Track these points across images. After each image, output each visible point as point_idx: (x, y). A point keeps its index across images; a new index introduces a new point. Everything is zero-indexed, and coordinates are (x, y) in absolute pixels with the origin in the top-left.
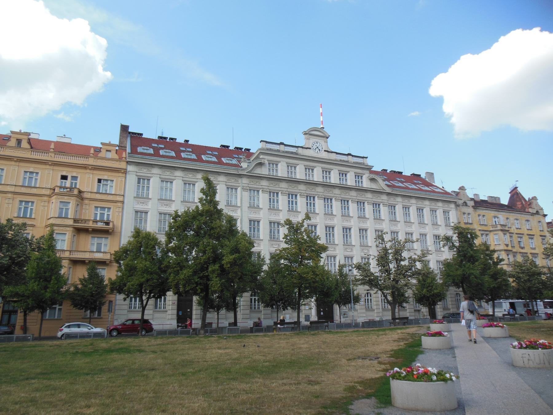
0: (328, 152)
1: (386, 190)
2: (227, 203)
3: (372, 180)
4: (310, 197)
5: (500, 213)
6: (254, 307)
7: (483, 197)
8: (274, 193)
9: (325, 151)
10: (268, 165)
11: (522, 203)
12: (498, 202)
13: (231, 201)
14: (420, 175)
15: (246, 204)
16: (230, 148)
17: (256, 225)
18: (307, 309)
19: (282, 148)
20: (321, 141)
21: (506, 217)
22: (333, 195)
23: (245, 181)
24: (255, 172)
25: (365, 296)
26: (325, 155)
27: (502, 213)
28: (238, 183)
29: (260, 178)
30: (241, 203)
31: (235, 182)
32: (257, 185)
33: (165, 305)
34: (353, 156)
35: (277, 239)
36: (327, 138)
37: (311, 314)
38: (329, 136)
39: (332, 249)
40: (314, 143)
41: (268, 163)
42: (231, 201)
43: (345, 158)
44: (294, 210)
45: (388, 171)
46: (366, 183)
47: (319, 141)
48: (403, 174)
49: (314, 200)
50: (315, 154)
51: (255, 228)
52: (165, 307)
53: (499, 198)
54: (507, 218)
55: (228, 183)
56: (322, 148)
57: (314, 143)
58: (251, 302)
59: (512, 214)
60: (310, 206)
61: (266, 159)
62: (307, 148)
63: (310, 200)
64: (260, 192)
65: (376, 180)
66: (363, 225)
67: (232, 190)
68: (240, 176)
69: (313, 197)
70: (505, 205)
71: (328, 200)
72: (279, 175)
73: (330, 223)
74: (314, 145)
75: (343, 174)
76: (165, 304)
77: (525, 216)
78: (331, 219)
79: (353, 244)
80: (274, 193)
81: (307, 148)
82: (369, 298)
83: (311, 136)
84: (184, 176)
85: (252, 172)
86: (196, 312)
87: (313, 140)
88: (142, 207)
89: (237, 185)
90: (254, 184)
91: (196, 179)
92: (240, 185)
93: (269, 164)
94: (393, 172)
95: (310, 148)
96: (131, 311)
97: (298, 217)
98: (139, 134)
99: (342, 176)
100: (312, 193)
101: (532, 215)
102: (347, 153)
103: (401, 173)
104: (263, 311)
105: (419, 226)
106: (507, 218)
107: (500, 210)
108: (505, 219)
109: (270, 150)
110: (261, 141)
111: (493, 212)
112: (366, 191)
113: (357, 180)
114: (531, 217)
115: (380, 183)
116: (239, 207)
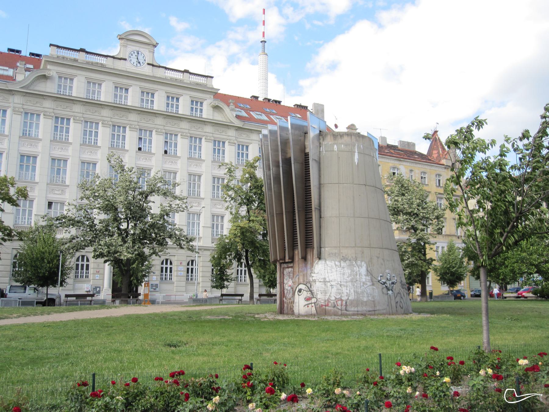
0: (153, 65)
1: (234, 123)
2: (112, 145)
3: (216, 108)
4: (219, 142)
5: (400, 163)
6: (165, 278)
7: (392, 141)
8: (196, 138)
9: (148, 64)
10: (57, 79)
11: (438, 153)
12: (411, 149)
13: (30, 131)
14: (307, 107)
15: (17, 132)
16: (259, 99)
17: (196, 180)
18: (98, 278)
19: (81, 57)
20: (145, 51)
21: (410, 168)
22: (153, 126)
23: (17, 100)
24: (37, 88)
25: (188, 264)
26: (147, 70)
27: (404, 163)
28: (8, 103)
29: (43, 96)
30: (10, 132)
31: (3, 101)
32: (36, 107)
33: (88, 274)
34: (88, 53)
35: (62, 183)
36: (155, 46)
37: (103, 286)
38: (157, 44)
39: (60, 192)
40: (132, 53)
41: (57, 77)
42: (30, 131)
43: (179, 76)
44: (120, 147)
45: (260, 99)
46: (207, 113)
47: (141, 50)
48: (282, 104)
49: (224, 146)
50: (134, 68)
51: (195, 184)
52: (88, 276)
53: (414, 145)
54: (411, 171)
55: (25, 106)
56: (145, 60)
57: (132, 53)
58: (162, 271)
59: (418, 166)
60: (243, 157)
61: (53, 71)
62: (120, 59)
63: (243, 150)
64: (42, 116)
65: (221, 108)
66: (172, 166)
67: (119, 128)
68: (11, 92)
69: (96, 123)
70: (421, 155)
71: (196, 141)
72: (74, 95)
73: (194, 169)
74: (132, 55)
75: (172, 98)
76: (88, 272)
77: (436, 169)
78: (32, 145)
79: (36, 181)
80: (196, 138)
81: (120, 59)
82: (85, 263)
83: (129, 43)
84: (55, 108)
85: (31, 88)
86: (93, 282)
87: (132, 47)
88: (90, 157)
89: (7, 105)
90: (31, 105)
91: (179, 128)
92: (11, 105)
93: (60, 77)
94: (267, 100)
95: (125, 59)
96: (239, 284)
97: (201, 166)
98: (276, 101)
99: (197, 105)
100: (123, 121)
101: (445, 168)
102: (79, 49)
103: (279, 102)
104: (201, 283)
105: (188, 161)
106: (411, 171)
107: (402, 159)
108: (408, 172)
109: (92, 64)
110: (51, 45)
111: (392, 162)
112: (204, 122)
113: (170, 102)
114: (444, 170)
115: (226, 113)
116: (7, 136)
